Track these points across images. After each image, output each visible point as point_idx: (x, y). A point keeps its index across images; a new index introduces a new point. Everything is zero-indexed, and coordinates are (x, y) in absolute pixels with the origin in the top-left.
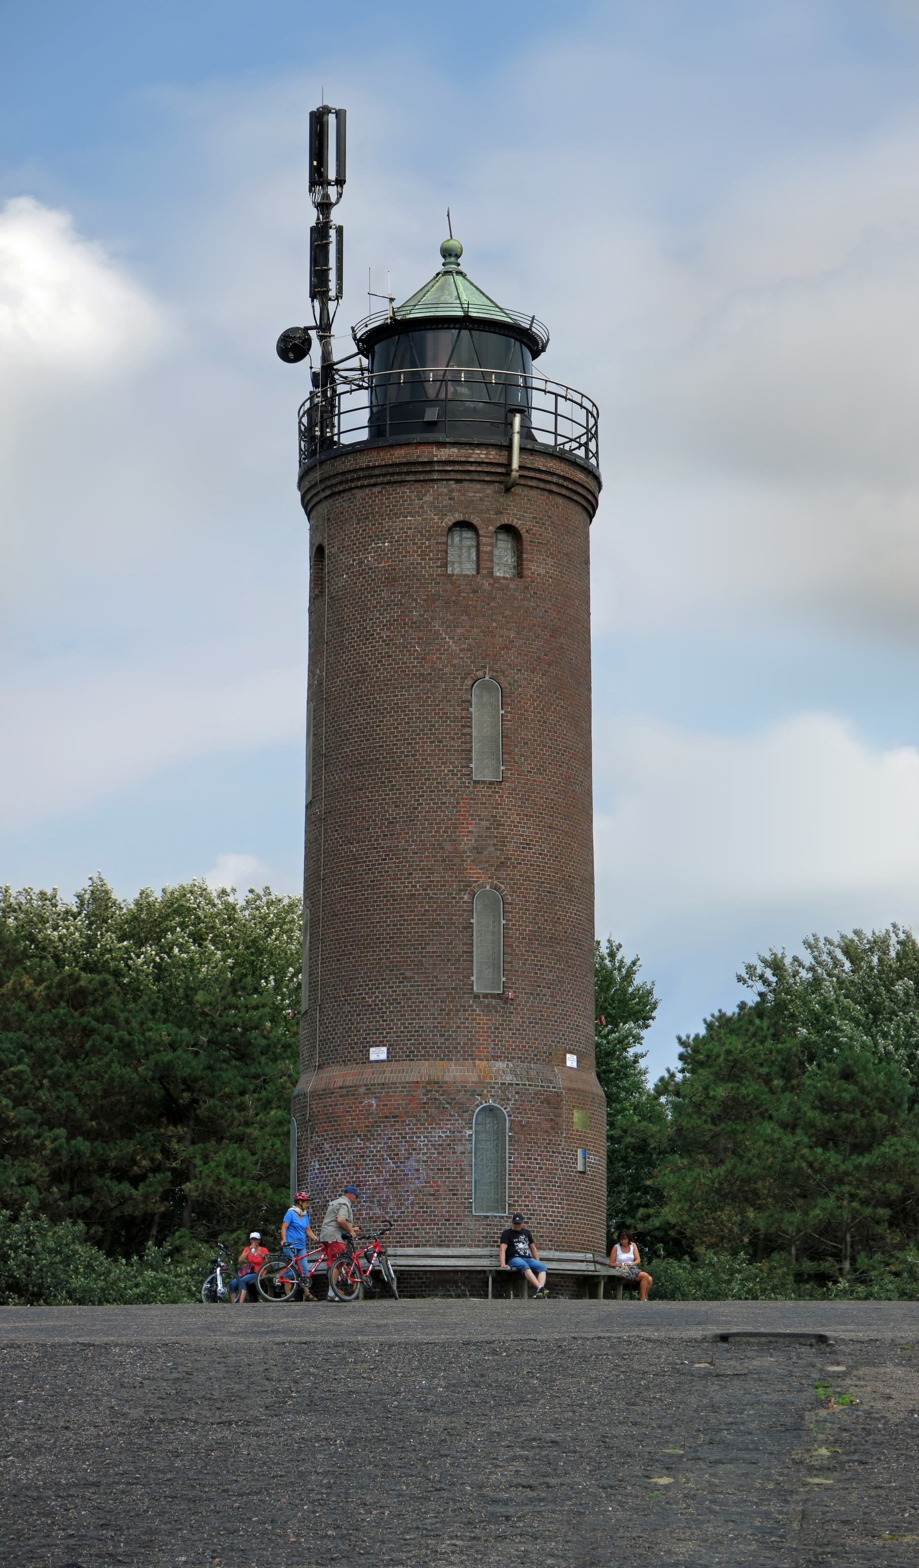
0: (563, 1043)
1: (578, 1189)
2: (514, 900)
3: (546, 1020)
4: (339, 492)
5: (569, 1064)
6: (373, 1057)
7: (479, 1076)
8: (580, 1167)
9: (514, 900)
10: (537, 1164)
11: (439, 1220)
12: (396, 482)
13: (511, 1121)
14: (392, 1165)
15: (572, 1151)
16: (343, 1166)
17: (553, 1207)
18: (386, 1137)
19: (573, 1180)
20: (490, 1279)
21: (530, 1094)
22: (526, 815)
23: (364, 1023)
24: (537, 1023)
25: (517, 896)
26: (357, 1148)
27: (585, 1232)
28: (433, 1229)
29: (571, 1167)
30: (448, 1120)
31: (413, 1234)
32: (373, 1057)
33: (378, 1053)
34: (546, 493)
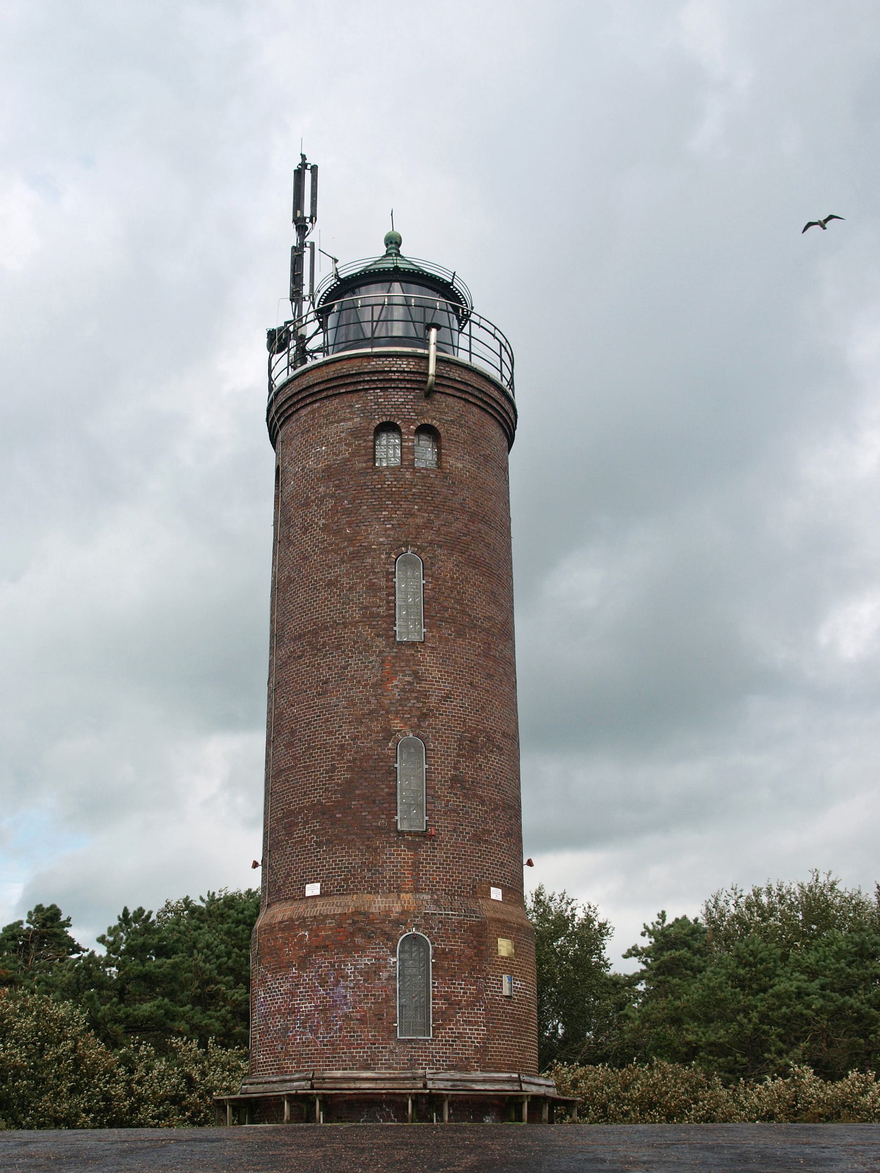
0: (487, 877)
1: (504, 1012)
2: (436, 747)
3: (469, 856)
4: (291, 415)
5: (493, 896)
6: (308, 893)
7: (403, 907)
8: (506, 992)
9: (436, 747)
10: (461, 989)
11: (365, 1044)
12: (331, 396)
13: (435, 949)
14: (322, 992)
15: (497, 976)
16: (281, 994)
17: (478, 1030)
18: (317, 966)
19: (499, 1004)
20: (410, 1102)
21: (454, 923)
22: (448, 672)
23: (302, 862)
24: (461, 858)
25: (439, 743)
26: (292, 977)
27: (512, 1053)
28: (360, 1052)
29: (496, 992)
30: (373, 948)
31: (341, 1057)
32: (308, 893)
33: (313, 889)
34: (463, 402)
